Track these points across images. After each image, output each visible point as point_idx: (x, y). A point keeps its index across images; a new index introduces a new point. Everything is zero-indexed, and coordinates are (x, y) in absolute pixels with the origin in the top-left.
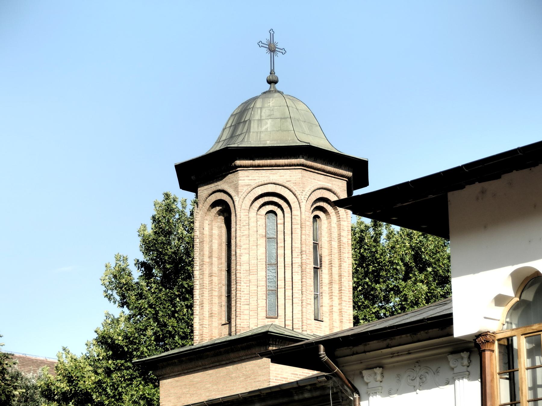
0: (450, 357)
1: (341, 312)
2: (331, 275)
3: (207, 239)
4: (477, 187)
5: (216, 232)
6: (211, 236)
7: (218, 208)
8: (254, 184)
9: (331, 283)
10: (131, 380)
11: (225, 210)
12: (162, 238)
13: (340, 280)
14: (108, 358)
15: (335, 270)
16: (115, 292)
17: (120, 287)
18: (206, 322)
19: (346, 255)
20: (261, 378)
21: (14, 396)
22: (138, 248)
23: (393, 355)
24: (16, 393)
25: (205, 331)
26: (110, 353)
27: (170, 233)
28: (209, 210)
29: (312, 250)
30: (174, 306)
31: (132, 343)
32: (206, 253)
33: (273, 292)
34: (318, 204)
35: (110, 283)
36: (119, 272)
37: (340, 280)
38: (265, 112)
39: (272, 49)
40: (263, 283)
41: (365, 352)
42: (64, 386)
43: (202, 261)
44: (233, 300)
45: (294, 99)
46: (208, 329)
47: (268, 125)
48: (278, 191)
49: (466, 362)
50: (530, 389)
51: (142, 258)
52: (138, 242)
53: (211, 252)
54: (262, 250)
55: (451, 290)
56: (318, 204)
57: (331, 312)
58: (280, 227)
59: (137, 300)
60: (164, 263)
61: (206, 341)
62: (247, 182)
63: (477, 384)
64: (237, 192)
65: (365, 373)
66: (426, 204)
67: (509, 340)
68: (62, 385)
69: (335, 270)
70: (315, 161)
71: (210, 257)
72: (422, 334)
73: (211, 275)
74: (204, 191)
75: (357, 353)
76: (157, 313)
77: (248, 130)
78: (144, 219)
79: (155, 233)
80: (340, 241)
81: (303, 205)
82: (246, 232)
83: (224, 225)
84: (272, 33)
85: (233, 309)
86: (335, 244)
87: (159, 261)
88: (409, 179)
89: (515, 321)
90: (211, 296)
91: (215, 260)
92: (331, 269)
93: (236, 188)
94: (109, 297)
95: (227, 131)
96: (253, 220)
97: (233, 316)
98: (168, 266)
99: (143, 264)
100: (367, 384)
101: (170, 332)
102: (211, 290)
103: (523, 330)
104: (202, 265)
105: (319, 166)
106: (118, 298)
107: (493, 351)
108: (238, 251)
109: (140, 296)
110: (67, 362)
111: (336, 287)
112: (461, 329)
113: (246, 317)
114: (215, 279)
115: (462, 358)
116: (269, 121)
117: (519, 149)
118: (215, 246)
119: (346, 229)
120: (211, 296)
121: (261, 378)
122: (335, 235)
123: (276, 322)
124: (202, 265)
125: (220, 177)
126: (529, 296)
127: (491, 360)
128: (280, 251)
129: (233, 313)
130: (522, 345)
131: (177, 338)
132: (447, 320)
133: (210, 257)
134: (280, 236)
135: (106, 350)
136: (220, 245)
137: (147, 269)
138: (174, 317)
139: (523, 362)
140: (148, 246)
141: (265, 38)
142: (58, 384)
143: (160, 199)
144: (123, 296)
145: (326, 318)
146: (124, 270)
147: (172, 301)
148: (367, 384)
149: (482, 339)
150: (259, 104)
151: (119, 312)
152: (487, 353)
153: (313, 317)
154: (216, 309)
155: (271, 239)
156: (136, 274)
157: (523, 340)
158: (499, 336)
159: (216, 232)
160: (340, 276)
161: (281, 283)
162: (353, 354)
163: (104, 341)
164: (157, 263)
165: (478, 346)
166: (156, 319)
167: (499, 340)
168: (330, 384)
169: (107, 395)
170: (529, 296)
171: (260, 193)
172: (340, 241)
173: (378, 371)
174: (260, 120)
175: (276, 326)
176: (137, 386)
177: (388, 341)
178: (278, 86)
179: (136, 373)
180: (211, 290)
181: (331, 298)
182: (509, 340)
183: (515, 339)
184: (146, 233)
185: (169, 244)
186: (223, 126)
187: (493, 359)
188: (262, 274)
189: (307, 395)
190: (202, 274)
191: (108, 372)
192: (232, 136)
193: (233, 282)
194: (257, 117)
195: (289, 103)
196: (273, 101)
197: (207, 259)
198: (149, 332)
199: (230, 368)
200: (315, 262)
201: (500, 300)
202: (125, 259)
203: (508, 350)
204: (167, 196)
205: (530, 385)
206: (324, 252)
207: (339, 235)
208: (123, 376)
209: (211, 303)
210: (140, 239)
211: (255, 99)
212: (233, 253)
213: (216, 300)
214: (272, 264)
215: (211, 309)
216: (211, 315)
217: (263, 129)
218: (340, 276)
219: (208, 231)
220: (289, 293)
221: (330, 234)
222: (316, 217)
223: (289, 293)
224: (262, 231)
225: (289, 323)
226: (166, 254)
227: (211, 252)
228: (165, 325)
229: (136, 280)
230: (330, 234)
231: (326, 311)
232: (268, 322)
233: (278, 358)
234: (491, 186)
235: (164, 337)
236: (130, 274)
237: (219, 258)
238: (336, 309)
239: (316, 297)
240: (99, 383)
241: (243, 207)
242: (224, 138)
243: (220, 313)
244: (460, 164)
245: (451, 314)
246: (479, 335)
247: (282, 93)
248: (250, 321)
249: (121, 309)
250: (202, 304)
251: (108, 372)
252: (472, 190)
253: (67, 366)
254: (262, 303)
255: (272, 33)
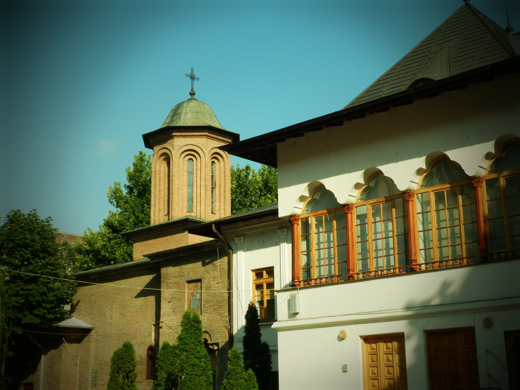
0: (278, 231)
1: (225, 210)
2: (220, 191)
3: (158, 172)
4: (292, 140)
5: (162, 169)
6: (160, 171)
7: (164, 157)
8: (182, 145)
9: (220, 195)
10: (120, 244)
11: (167, 158)
12: (138, 174)
13: (225, 194)
14: (109, 233)
15: (222, 189)
16: (114, 200)
17: (116, 197)
18: (157, 214)
19: (228, 181)
20: (184, 242)
21: (59, 250)
22: (126, 179)
23: (249, 230)
24: (60, 248)
25: (157, 218)
26: (111, 230)
27: (142, 171)
28: (159, 158)
29: (211, 178)
30: (143, 208)
31: (122, 225)
32: (158, 179)
33: (191, 200)
34: (214, 156)
35: (112, 196)
36: (116, 190)
37: (225, 194)
38: (188, 109)
39: (192, 78)
40: (186, 195)
41: (235, 228)
42: (87, 247)
43: (155, 183)
44: (171, 203)
45: (203, 103)
46: (157, 217)
47: (190, 115)
48: (194, 149)
49: (286, 233)
50: (317, 244)
51: (128, 184)
52: (126, 175)
53: (160, 179)
54: (185, 178)
55: (316, 286)
56: (214, 156)
57: (220, 209)
58: (195, 167)
59: (125, 204)
60: (139, 186)
61: (157, 224)
62: (178, 144)
63: (290, 245)
64: (173, 149)
65: (235, 238)
66: (265, 148)
67: (307, 219)
68: (86, 247)
69: (222, 189)
70: (213, 134)
71: (160, 181)
72: (264, 219)
73: (160, 191)
74: (156, 148)
75: (232, 229)
76: (134, 211)
77: (180, 118)
78: (129, 164)
79: (134, 171)
80: (225, 174)
81: (206, 156)
82: (178, 169)
83: (166, 165)
84: (192, 69)
85: (171, 207)
86: (222, 176)
87: (136, 185)
88: (257, 136)
89: (310, 209)
90: (160, 201)
91: (162, 183)
92: (220, 188)
93: (173, 147)
94: (111, 203)
95: (169, 118)
96: (181, 163)
97: (170, 211)
98: (141, 188)
99: (128, 187)
100: (236, 244)
101: (141, 221)
102: (160, 198)
103: (313, 214)
104: (155, 185)
105: (215, 136)
106: (115, 203)
107: (298, 224)
108: (173, 179)
109: (126, 202)
110: (88, 234)
111: (222, 197)
112: (281, 214)
113: (177, 211)
114: (162, 193)
115: (284, 231)
116: (190, 114)
117: (313, 119)
118: (162, 176)
119: (228, 168)
120: (160, 201)
121: (184, 242)
122: (222, 171)
123: (192, 214)
124: (155, 185)
125: (165, 141)
126: (317, 196)
127: (297, 229)
128: (195, 179)
129: (170, 209)
130: (313, 221)
131: (144, 223)
132: (275, 212)
133: (160, 181)
134: (195, 171)
135: (108, 229)
136: (165, 175)
137: (131, 190)
138: (143, 213)
139: (313, 230)
140: (131, 177)
141: (189, 72)
142: (84, 246)
143: (138, 154)
144: (118, 202)
145: (217, 213)
146: (118, 189)
147: (142, 206)
148: (236, 244)
149: (293, 218)
150: (185, 105)
151: (116, 210)
152: (295, 226)
153: (210, 212)
154: (162, 207)
155: (190, 173)
156: (125, 191)
157: (314, 219)
158: (302, 217)
159: (162, 169)
160: (225, 192)
161: (195, 195)
162: (229, 229)
163: (109, 224)
164: (135, 186)
165: (290, 222)
166: (134, 214)
167: (301, 219)
168: (218, 244)
169: (108, 252)
170: (317, 196)
171: (185, 149)
172: (225, 174)
173: (242, 238)
174: (186, 113)
175: (192, 216)
176: (124, 247)
177: (247, 223)
178: (195, 96)
179: (123, 241)
180: (160, 198)
181: (220, 203)
182: (307, 219)
183: (310, 218)
184: (130, 171)
185: (142, 177)
186: (167, 116)
187: (298, 229)
188: (185, 190)
189: (206, 250)
190: (155, 190)
191: (110, 239)
192: (172, 121)
193: (171, 194)
194: (184, 111)
195: (201, 105)
196: (192, 104)
197: (157, 183)
198: (131, 220)
199: (169, 237)
200: (212, 185)
201: (302, 198)
202: (119, 184)
203: (306, 225)
204: (141, 153)
205: (317, 242)
206: (217, 179)
207: (225, 171)
208: (117, 242)
209: (159, 204)
210: (127, 174)
211: (183, 103)
212: (171, 179)
213: (162, 203)
214: (191, 185)
215: (159, 208)
216: (159, 211)
217: (187, 117)
218: (225, 192)
219: (158, 168)
220: (199, 200)
221: (220, 170)
222: (213, 162)
223: (199, 200)
224: (185, 169)
225: (198, 214)
226: (140, 182)
227: (160, 179)
228: (138, 217)
229: (125, 195)
230: (220, 170)
231: (217, 208)
232: (188, 214)
233: (193, 231)
234: (299, 140)
235: (138, 223)
236: (121, 192)
237: (164, 182)
238: (222, 208)
239: (212, 202)
240: (104, 245)
241: (176, 156)
242: (167, 122)
243: (164, 209)
244: (283, 128)
245: (278, 209)
246: (291, 216)
247: (197, 100)
248: (179, 213)
249: (117, 209)
250: (155, 205)
251: (110, 239)
252: (290, 141)
253: (89, 237)
254: (185, 204)
255: (192, 69)
